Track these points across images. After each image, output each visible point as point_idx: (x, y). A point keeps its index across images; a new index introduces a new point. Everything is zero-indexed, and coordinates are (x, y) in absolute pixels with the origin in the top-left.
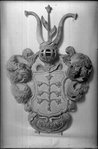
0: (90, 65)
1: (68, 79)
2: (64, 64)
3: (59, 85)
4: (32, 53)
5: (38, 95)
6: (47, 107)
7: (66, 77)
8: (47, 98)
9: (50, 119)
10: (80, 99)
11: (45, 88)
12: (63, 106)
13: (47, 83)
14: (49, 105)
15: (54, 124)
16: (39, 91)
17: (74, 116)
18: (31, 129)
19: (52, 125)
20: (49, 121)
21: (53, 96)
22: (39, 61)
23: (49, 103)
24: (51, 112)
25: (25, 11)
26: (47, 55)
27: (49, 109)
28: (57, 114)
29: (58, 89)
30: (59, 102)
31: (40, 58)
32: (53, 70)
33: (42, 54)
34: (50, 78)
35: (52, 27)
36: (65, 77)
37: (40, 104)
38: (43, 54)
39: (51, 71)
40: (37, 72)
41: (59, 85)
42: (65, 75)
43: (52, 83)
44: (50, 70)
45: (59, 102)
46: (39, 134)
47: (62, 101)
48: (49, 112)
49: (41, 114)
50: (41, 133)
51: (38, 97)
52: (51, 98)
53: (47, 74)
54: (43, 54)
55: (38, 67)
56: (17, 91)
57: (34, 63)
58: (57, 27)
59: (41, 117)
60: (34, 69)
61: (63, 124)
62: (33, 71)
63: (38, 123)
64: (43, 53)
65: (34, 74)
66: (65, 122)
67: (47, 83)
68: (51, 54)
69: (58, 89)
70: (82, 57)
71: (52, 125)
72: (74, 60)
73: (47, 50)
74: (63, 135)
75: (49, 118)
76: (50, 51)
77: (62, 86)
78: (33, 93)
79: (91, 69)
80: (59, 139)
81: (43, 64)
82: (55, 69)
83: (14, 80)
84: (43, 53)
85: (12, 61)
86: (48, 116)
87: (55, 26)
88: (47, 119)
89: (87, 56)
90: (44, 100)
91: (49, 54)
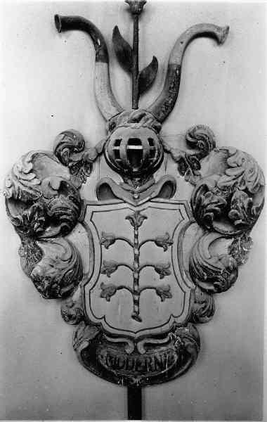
0: (257, 185)
1: (193, 225)
2: (181, 181)
3: (162, 243)
4: (81, 146)
5: (104, 272)
6: (131, 308)
7: (187, 220)
8: (130, 284)
9: (140, 345)
11: (120, 253)
12: (179, 306)
13: (131, 238)
14: (136, 302)
16: (104, 261)
19: (146, 360)
20: (136, 348)
21: (149, 277)
22: (101, 172)
23: (136, 276)
24: (140, 323)
25: (57, 17)
27: (136, 317)
28: (158, 331)
29: (162, 256)
30: (164, 294)
31: (107, 160)
32: (148, 199)
34: (136, 221)
35: (144, 62)
37: (128, 218)
38: (119, 151)
39: (141, 202)
40: (100, 203)
41: (162, 243)
42: (185, 215)
43: (144, 239)
44: (138, 198)
45: (164, 294)
47: (175, 291)
48: (135, 325)
51: (103, 277)
52: (142, 283)
53: (127, 209)
54: (119, 151)
55: (104, 189)
56: (246, 190)
58: (162, 62)
59: (109, 339)
60: (88, 191)
61: (176, 357)
62: (88, 201)
63: (102, 357)
64: (117, 148)
65: (90, 209)
67: (131, 238)
69: (162, 256)
71: (146, 360)
73: (132, 142)
75: (135, 341)
77: (175, 245)
78: (87, 269)
79: (207, 214)
81: (118, 179)
82: (153, 195)
84: (117, 148)
85: (27, 172)
86: (132, 335)
87: (155, 60)
88: (131, 344)
90: (121, 288)
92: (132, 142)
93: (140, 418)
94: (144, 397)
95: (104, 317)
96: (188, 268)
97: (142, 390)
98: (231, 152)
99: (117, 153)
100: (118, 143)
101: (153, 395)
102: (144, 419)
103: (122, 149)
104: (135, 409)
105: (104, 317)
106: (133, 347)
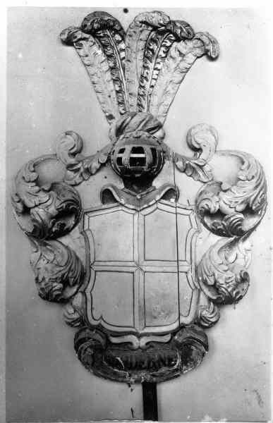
22: (106, 179)
38: (121, 158)
40: (104, 207)
54: (121, 158)
64: (120, 155)
73: (135, 150)
84: (120, 155)
92: (135, 150)
93: (156, 419)
94: (160, 404)
95: (101, 318)
96: (83, 286)
97: (158, 387)
98: (153, 306)
99: (119, 160)
100: (122, 151)
101: (167, 392)
102: (161, 421)
103: (125, 157)
104: (151, 407)
105: (101, 318)
106: (197, 40)
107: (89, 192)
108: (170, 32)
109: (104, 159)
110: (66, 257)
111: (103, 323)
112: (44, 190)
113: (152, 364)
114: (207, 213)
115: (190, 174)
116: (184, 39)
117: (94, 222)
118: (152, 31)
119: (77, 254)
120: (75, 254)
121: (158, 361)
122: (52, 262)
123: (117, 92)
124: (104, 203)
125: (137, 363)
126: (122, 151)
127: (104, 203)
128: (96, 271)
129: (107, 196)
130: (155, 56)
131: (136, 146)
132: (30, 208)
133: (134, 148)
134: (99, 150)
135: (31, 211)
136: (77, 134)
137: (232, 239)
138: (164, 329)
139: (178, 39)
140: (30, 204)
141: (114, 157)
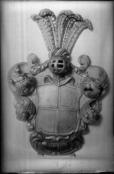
10: (36, 19)
15: (61, 144)
17: (86, 137)
18: (33, 151)
22: (48, 72)
26: (59, 66)
33: (53, 66)
36: (61, 47)
38: (54, 65)
40: (45, 84)
46: (75, 157)
49: (48, 133)
50: (44, 155)
57: (39, 73)
64: (54, 63)
66: (75, 148)
68: (64, 66)
70: (102, 72)
72: (93, 73)
74: (76, 157)
76: (63, 63)
80: (66, 162)
83: (83, 89)
89: (106, 73)
91: (61, 66)
95: (41, 128)
107: (40, 78)
108: (73, 18)
109: (46, 65)
110: (29, 103)
111: (42, 131)
112: (21, 76)
113: (61, 148)
114: (86, 89)
115: (79, 73)
116: (79, 21)
117: (40, 90)
118: (66, 17)
119: (33, 102)
120: (32, 102)
121: (63, 147)
122: (23, 105)
123: (52, 40)
124: (45, 83)
125: (60, 147)
126: (54, 62)
127: (45, 83)
128: (40, 109)
129: (46, 79)
130: (67, 27)
131: (60, 60)
132: (15, 82)
133: (59, 60)
134: (89, 19)
135: (16, 83)
136: (35, 55)
137: (94, 99)
138: (66, 134)
139: (77, 21)
140: (15, 81)
141: (50, 64)
